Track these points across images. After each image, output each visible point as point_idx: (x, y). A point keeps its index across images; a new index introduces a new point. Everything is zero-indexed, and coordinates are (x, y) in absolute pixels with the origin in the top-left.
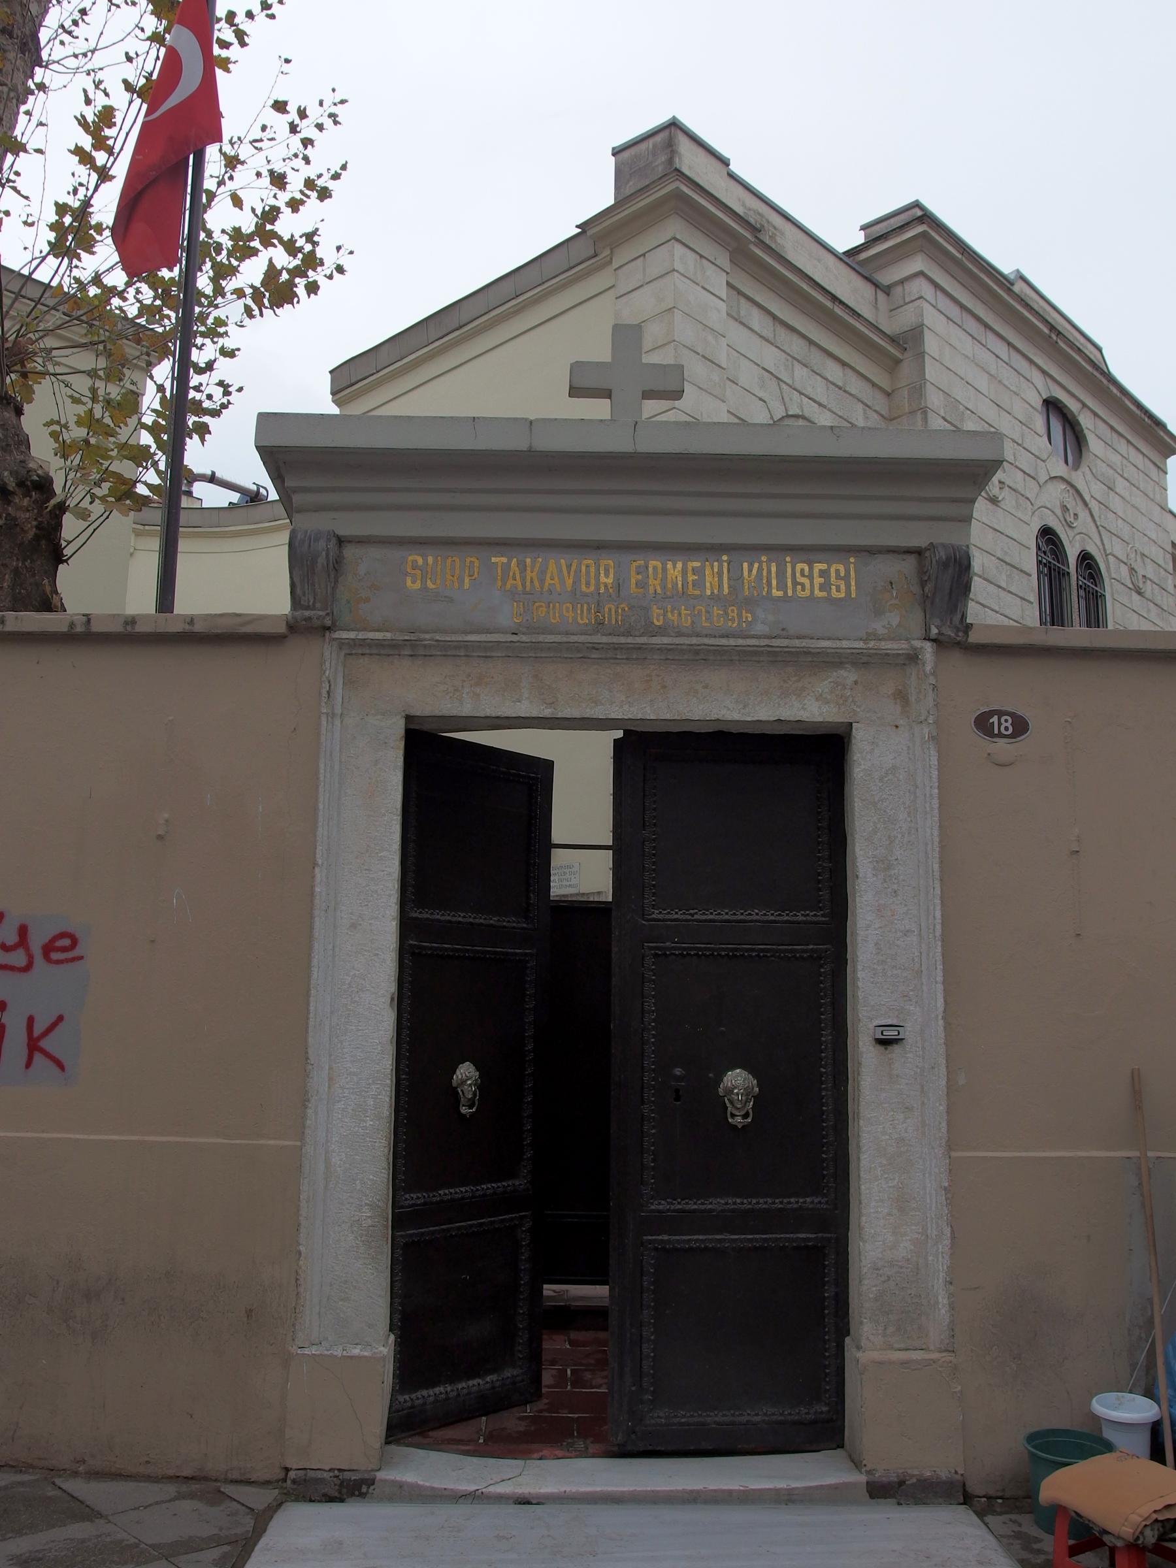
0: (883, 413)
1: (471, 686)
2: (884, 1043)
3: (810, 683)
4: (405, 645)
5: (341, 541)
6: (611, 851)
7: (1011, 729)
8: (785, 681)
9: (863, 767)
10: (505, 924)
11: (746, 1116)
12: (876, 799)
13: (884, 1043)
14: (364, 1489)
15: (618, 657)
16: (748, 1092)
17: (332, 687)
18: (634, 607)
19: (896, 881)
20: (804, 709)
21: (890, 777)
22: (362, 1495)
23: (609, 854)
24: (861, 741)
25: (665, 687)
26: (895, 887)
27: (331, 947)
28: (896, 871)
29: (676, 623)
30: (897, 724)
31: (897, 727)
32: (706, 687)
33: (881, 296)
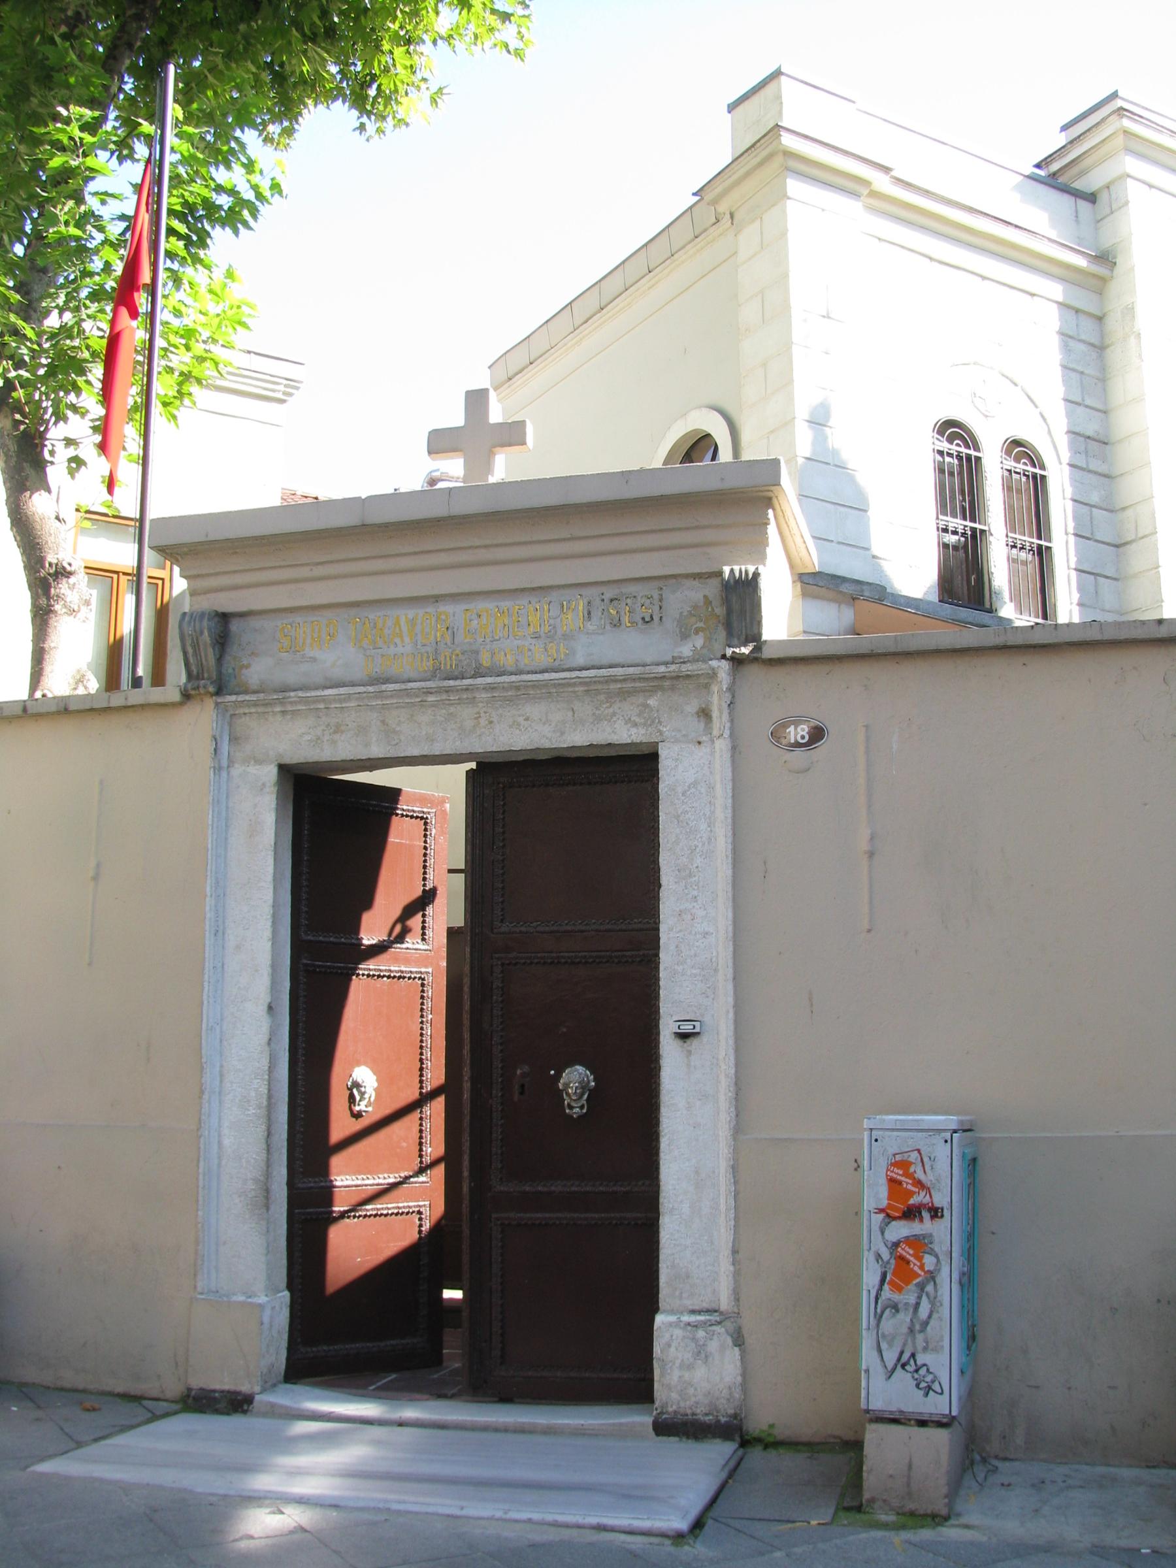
0: (1093, 341)
1: (330, 735)
2: (684, 1036)
3: (620, 708)
4: (275, 703)
5: (224, 618)
6: (463, 875)
7: (807, 738)
8: (597, 708)
9: (667, 783)
10: (353, 941)
11: (582, 1107)
12: (679, 812)
13: (684, 1036)
14: (245, 1407)
15: (452, 698)
16: (584, 1086)
17: (219, 744)
18: (466, 651)
19: (696, 888)
20: (615, 733)
21: (693, 790)
22: (245, 1412)
23: (463, 875)
24: (666, 759)
25: (491, 722)
26: (695, 893)
27: (220, 964)
28: (697, 878)
29: (502, 662)
30: (700, 739)
31: (699, 743)
32: (527, 719)
33: (1083, 205)
